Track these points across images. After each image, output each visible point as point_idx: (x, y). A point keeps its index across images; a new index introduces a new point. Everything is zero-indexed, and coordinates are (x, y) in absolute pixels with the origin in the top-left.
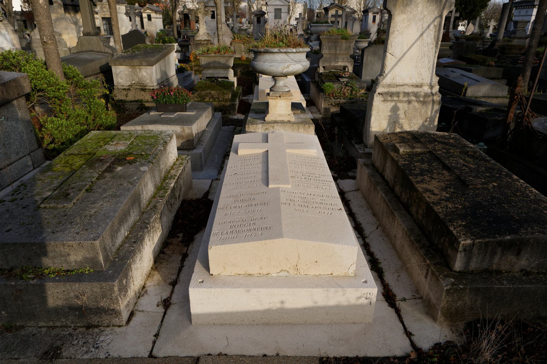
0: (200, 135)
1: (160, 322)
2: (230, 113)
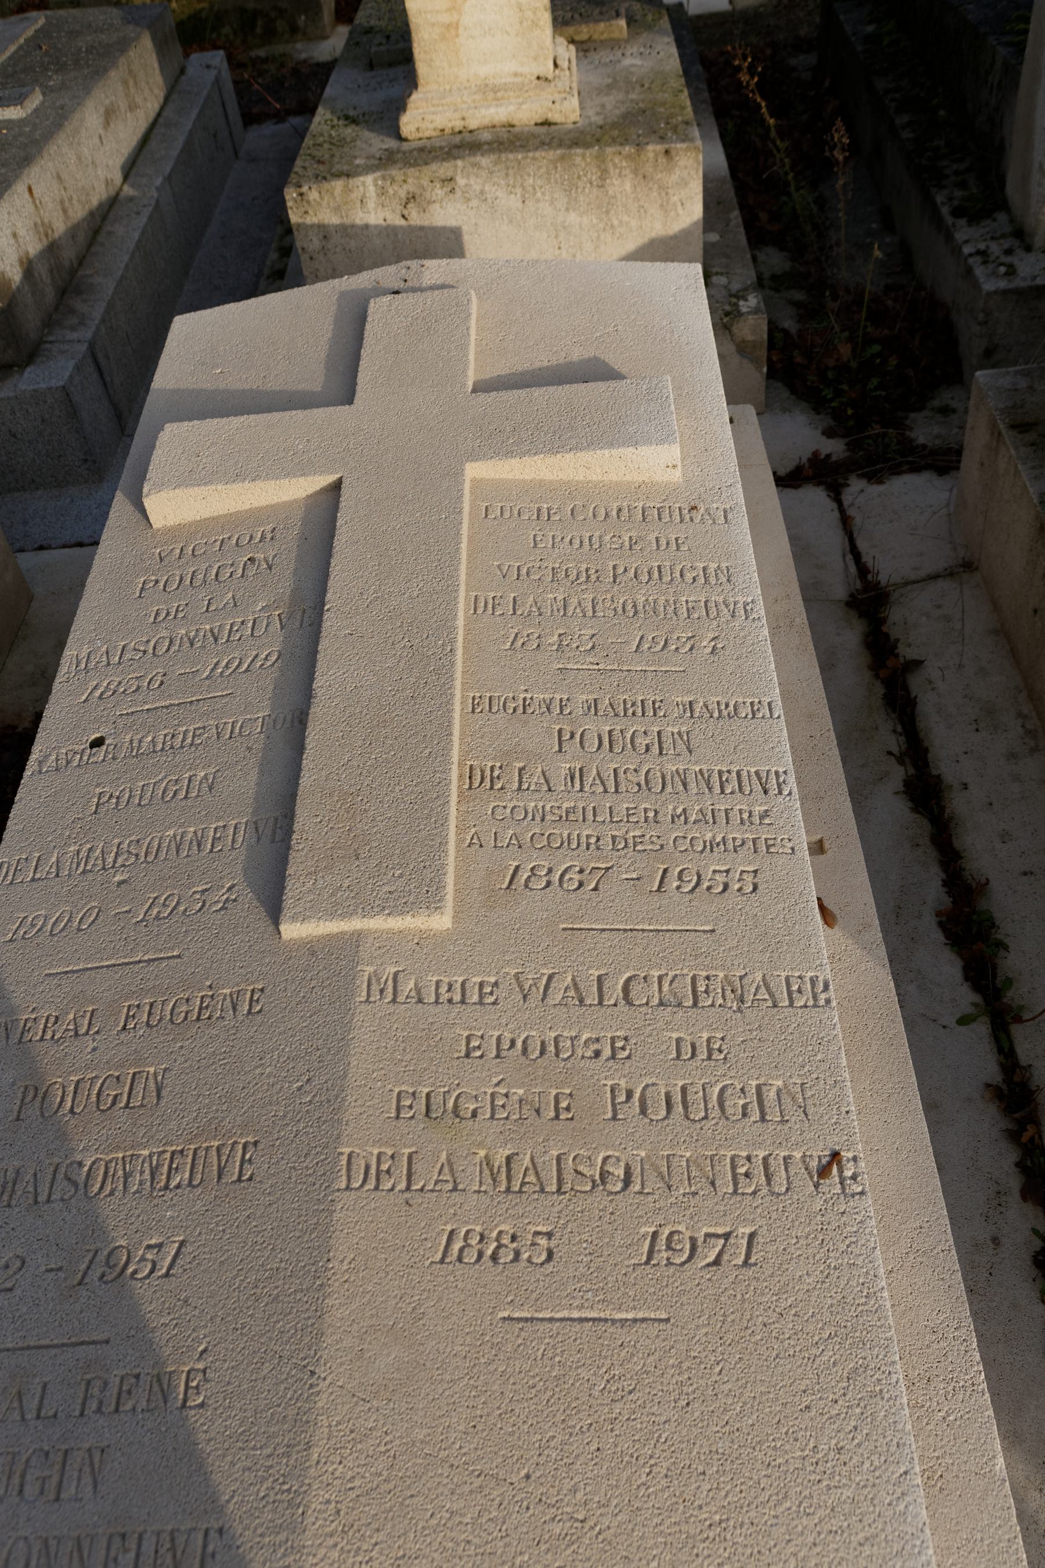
0: (69, 255)
2: (294, 29)
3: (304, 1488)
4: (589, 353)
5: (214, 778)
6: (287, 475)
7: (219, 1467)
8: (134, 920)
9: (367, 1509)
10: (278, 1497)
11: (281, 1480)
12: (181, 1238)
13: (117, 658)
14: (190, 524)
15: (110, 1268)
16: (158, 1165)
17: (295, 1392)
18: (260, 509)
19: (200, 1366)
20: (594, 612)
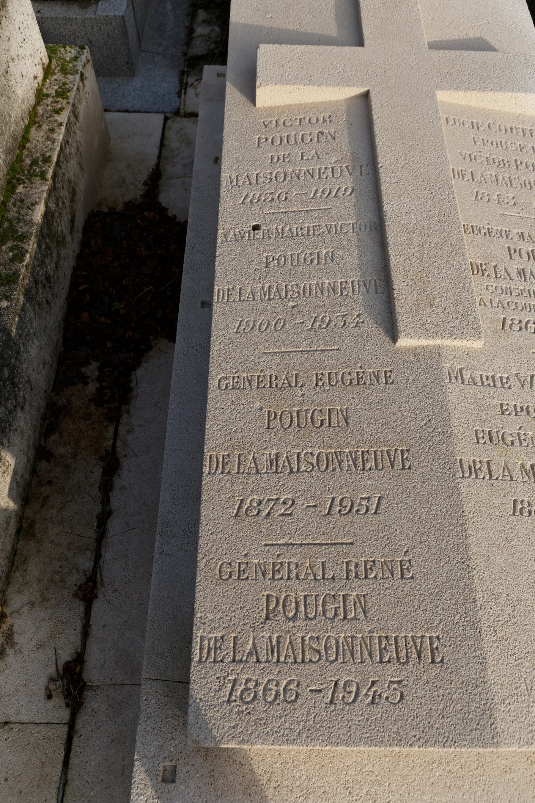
1: (60, 766)
3: (478, 620)
4: (477, 35)
5: (332, 254)
6: (338, 85)
7: (430, 607)
8: (307, 328)
9: (508, 630)
10: (465, 623)
11: (464, 616)
12: (379, 495)
13: (255, 181)
14: (279, 107)
15: (344, 507)
16: (356, 458)
17: (461, 574)
18: (319, 103)
19: (407, 558)
20: (511, 185)
